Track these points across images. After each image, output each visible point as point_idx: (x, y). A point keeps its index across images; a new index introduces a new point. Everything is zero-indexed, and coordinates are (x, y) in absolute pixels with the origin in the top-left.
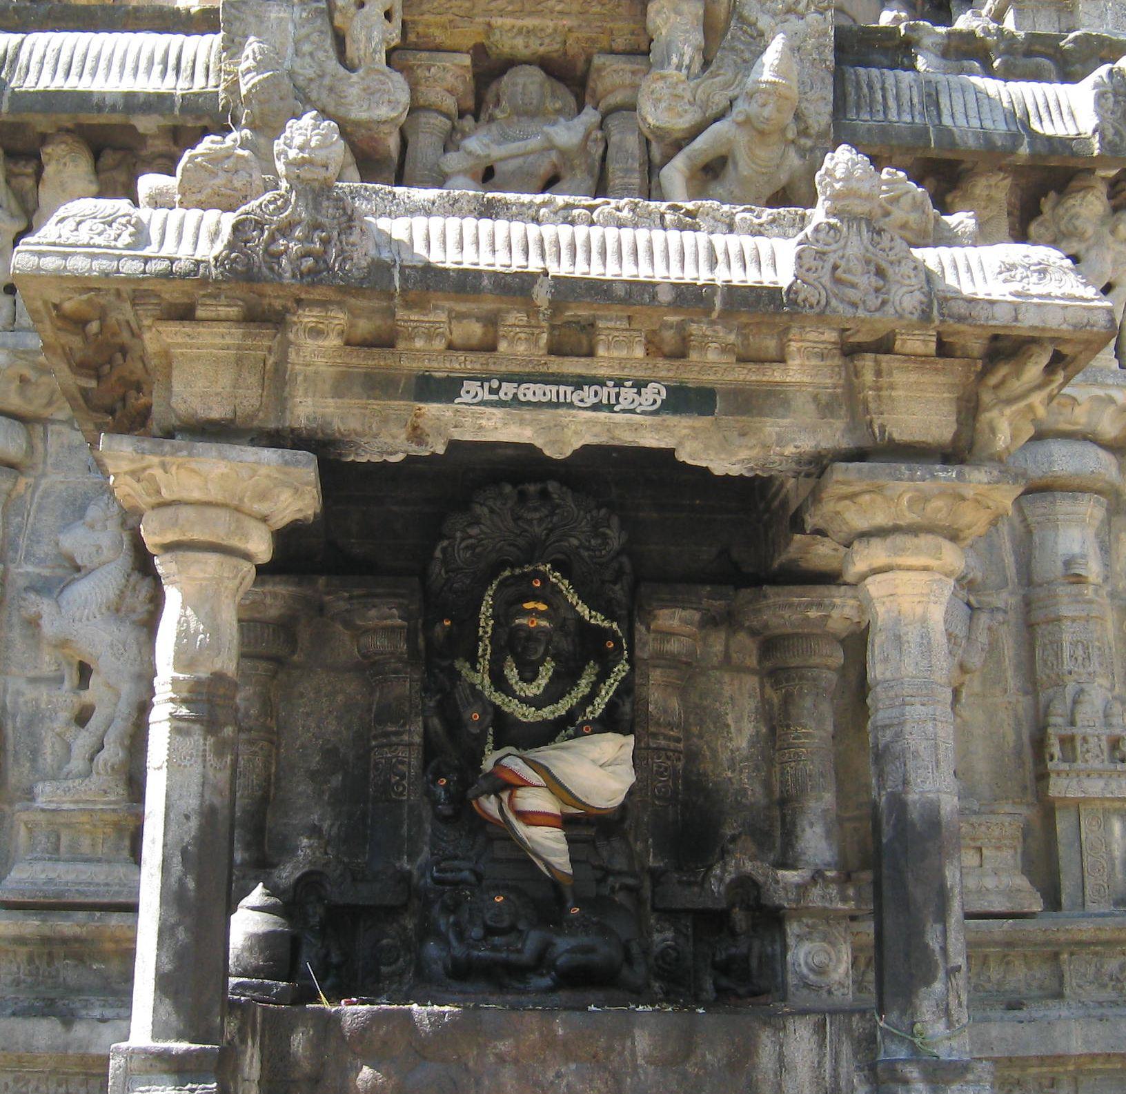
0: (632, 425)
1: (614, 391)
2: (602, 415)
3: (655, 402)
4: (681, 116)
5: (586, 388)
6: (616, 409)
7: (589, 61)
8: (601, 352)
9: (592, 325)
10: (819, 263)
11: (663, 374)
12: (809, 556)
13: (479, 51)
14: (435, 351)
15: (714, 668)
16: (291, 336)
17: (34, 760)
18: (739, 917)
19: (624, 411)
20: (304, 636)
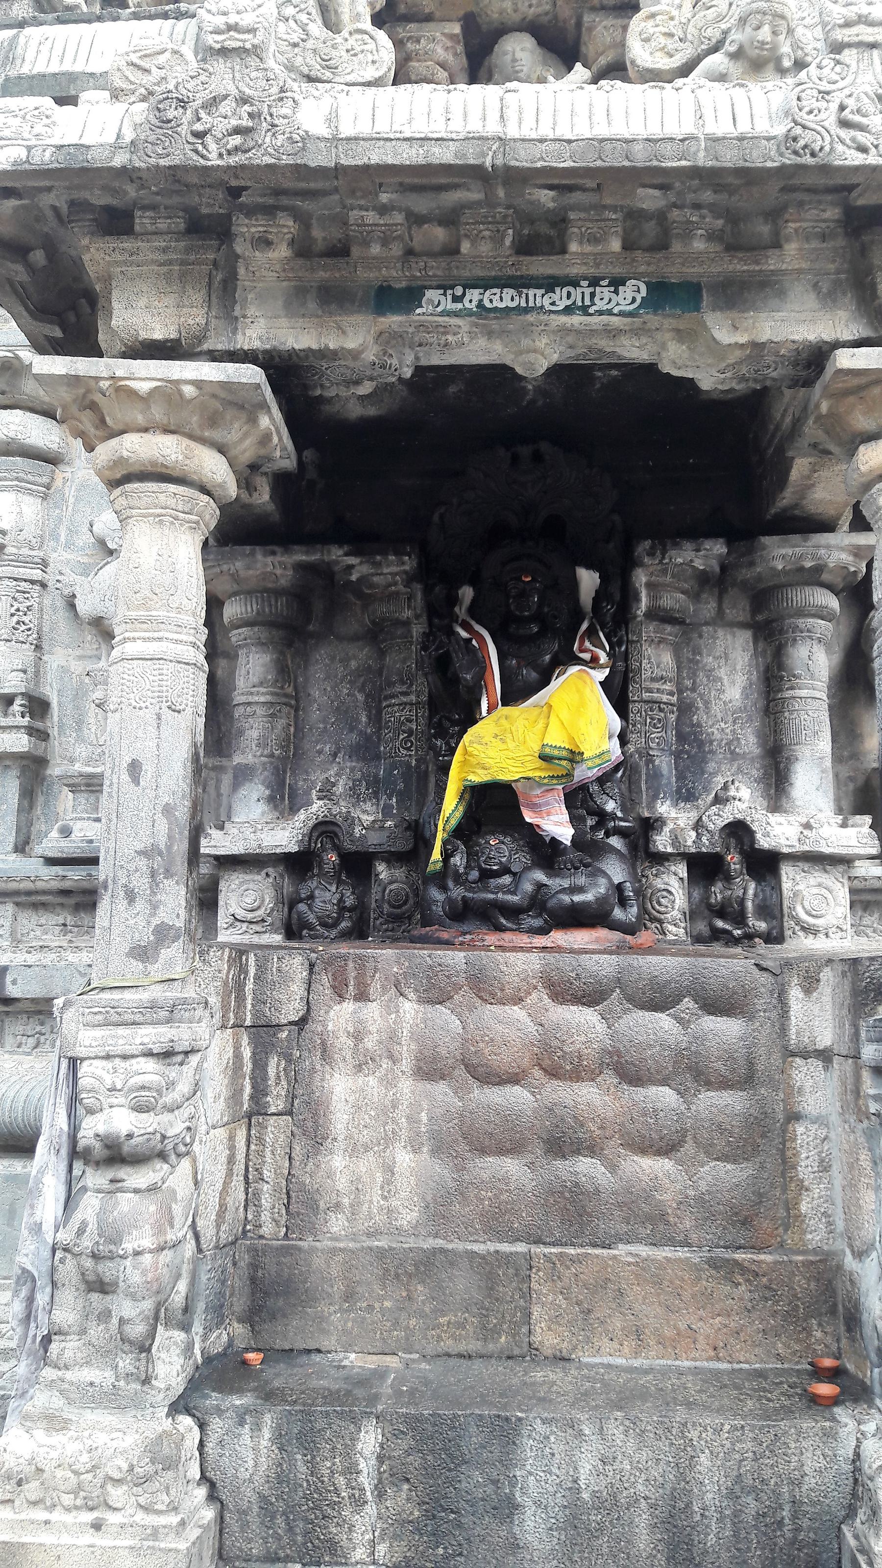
0: (610, 331)
1: (588, 291)
2: (576, 320)
3: (634, 300)
4: (671, 56)
5: (557, 290)
6: (591, 310)
7: (579, 24)
8: (574, 247)
9: (564, 220)
10: (823, 104)
11: (643, 268)
12: (804, 502)
13: (470, 22)
14: (392, 257)
15: (707, 624)
16: (239, 249)
17: (79, 729)
18: (734, 860)
19: (600, 313)
20: (318, 606)
